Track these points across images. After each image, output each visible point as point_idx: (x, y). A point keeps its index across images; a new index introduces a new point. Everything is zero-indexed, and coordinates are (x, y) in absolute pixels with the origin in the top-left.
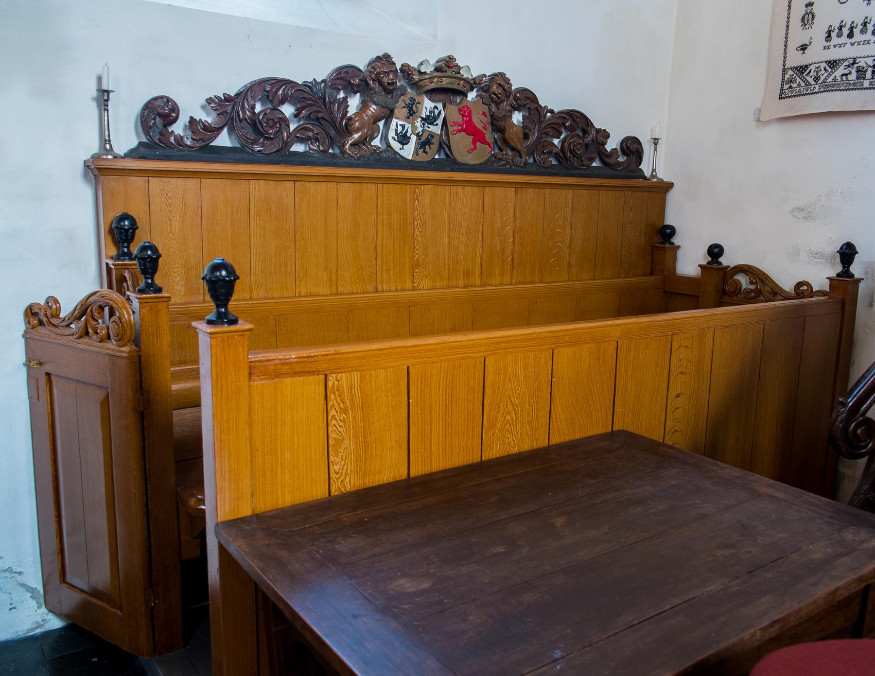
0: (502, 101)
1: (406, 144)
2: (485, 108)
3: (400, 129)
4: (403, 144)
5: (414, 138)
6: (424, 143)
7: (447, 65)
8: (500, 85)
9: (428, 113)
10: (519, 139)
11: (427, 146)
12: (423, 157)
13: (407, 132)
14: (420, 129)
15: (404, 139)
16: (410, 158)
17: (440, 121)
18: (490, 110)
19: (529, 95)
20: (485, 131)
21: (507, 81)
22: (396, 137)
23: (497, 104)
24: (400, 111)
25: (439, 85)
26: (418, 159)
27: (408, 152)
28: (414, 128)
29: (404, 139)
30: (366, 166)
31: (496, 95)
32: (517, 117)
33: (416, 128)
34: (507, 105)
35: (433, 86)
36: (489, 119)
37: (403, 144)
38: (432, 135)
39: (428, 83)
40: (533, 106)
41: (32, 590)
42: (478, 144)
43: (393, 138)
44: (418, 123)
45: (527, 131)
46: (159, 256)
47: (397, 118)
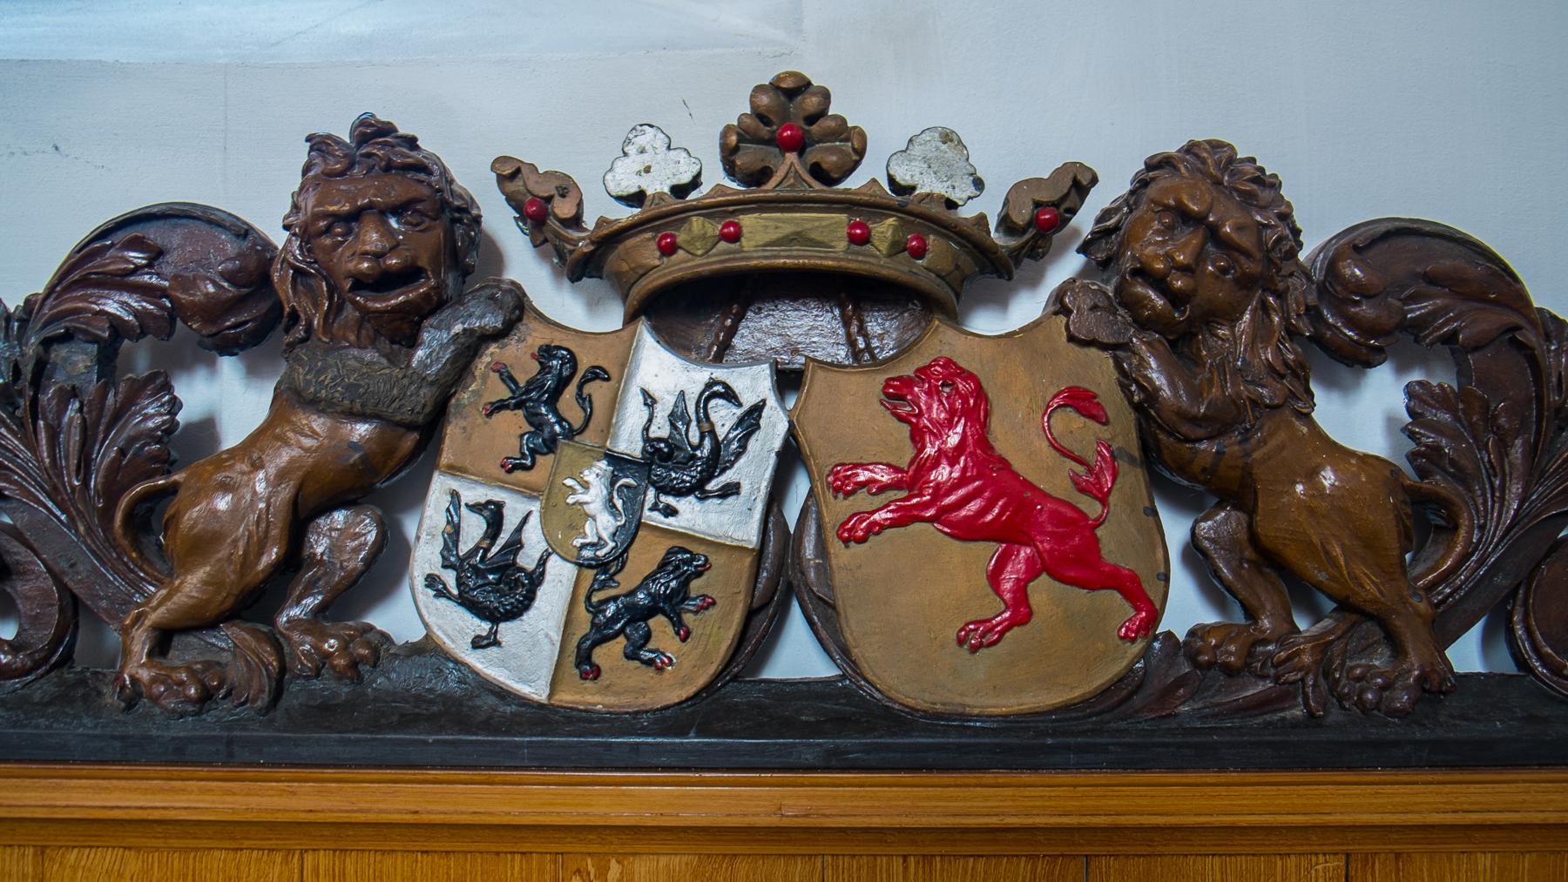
0: (1212, 316)
1: (515, 613)
2: (1099, 372)
3: (473, 528)
4: (495, 617)
5: (560, 578)
6: (625, 611)
7: (374, 170)
8: (1184, 216)
9: (661, 429)
10: (1368, 542)
11: (658, 623)
12: (622, 686)
13: (515, 545)
14: (603, 525)
15: (496, 587)
16: (536, 690)
17: (753, 470)
18: (1126, 379)
19: (1446, 262)
20: (1092, 508)
21: (1259, 188)
22: (450, 578)
23: (1180, 342)
24: (483, 431)
25: (718, 258)
26: (566, 697)
27: (525, 658)
28: (564, 518)
29: (496, 587)
30: (229, 754)
31: (1159, 283)
32: (1365, 414)
33: (581, 514)
34: (1261, 333)
35: (681, 265)
36: (1123, 429)
37: (495, 617)
38: (685, 561)
39: (651, 255)
40: (1476, 323)
41: (1353, 625)
42: (1043, 591)
43: (432, 581)
44: (592, 489)
45: (1439, 483)
46: (1481, 279)
47: (454, 470)
